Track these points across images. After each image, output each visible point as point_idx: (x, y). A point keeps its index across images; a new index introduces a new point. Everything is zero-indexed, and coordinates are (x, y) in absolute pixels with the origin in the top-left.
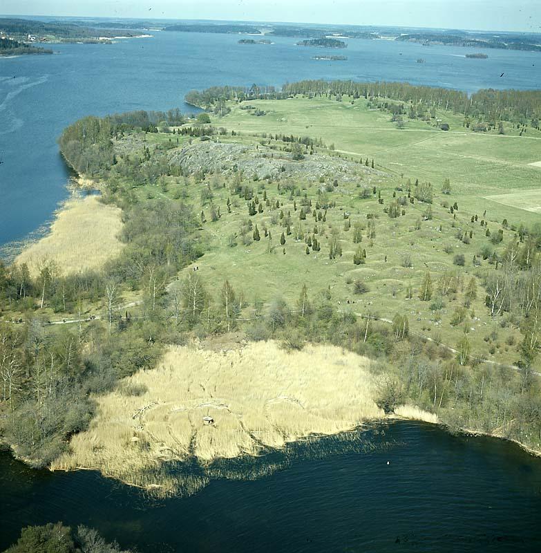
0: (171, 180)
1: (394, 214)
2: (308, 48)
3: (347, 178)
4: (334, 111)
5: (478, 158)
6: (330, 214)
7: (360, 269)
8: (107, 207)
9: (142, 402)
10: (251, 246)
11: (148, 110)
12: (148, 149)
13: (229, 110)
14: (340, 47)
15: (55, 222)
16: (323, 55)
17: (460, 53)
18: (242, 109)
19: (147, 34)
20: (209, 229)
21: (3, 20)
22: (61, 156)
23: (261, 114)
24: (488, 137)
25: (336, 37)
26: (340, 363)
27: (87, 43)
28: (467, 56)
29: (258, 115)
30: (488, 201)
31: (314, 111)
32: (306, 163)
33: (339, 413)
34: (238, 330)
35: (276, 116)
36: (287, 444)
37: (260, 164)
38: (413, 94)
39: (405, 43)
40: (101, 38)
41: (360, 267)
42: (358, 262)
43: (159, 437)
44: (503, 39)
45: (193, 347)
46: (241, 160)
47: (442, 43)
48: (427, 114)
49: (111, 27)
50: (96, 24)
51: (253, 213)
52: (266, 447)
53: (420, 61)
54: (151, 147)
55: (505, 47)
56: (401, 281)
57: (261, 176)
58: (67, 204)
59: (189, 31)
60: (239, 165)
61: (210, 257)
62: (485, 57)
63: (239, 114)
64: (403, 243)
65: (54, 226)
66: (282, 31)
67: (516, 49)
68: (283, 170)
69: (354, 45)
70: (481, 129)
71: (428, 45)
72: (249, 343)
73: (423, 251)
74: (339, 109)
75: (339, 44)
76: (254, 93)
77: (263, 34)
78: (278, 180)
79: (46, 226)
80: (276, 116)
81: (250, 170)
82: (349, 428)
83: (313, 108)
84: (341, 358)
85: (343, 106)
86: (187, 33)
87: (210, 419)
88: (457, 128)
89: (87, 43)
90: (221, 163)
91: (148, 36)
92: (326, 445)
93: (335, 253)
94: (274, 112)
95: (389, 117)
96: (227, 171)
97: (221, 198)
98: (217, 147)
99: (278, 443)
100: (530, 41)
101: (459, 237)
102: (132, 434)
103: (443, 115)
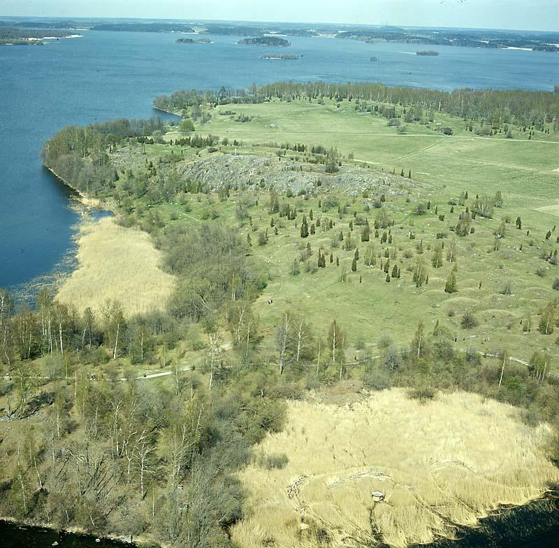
0: (192, 198)
1: (462, 233)
2: (250, 47)
3: (393, 193)
4: (322, 116)
5: (500, 165)
6: (393, 231)
7: (455, 299)
8: (130, 230)
9: (290, 476)
10: (318, 274)
11: (130, 118)
12: (151, 163)
13: (209, 115)
14: (285, 46)
15: (79, 250)
16: (273, 55)
17: (411, 50)
18: (222, 114)
19: (77, 34)
20: (260, 254)
21: (3, 24)
22: (46, 171)
23: (246, 120)
24: (497, 141)
25: (273, 34)
26: (484, 413)
27: (16, 44)
28: (418, 54)
29: (243, 122)
30: (542, 214)
31: (301, 116)
32: (344, 176)
33: (519, 478)
34: (349, 377)
35: (263, 122)
36: (481, 520)
37: (291, 177)
38: (402, 95)
39: (345, 40)
40: (30, 39)
41: (455, 296)
42: (450, 289)
43: (333, 521)
44: (445, 35)
45: (311, 401)
46: (267, 174)
47: (384, 40)
48: (424, 117)
49: (34, 27)
50: (18, 24)
51: (305, 235)
52: (460, 526)
53: (373, 59)
54: (154, 160)
55: (450, 44)
56: (508, 312)
57: (296, 191)
58: (83, 229)
59: (119, 30)
60: (265, 179)
61: (277, 288)
62: (436, 54)
63: (221, 121)
64: (489, 266)
65: (80, 255)
66: (216, 29)
67: (462, 45)
68: (319, 184)
69: (297, 44)
70: (486, 133)
71: (372, 42)
72: (371, 393)
73: (516, 275)
74: (325, 113)
75: (283, 43)
76: (223, 97)
77: (197, 32)
78: (316, 196)
79: (70, 255)
80: (263, 122)
81: (281, 184)
82: (538, 496)
83: (300, 112)
84: (480, 406)
85: (328, 109)
86: (117, 32)
87: (381, 495)
88: (460, 132)
89: (16, 44)
90: (245, 178)
91: (77, 36)
92: (525, 519)
93: (419, 280)
94: (259, 117)
95: (385, 122)
96: (253, 186)
97: (261, 218)
98: (236, 160)
99: (471, 521)
100: (472, 37)
101: (543, 257)
102: (299, 520)
103: (442, 119)
